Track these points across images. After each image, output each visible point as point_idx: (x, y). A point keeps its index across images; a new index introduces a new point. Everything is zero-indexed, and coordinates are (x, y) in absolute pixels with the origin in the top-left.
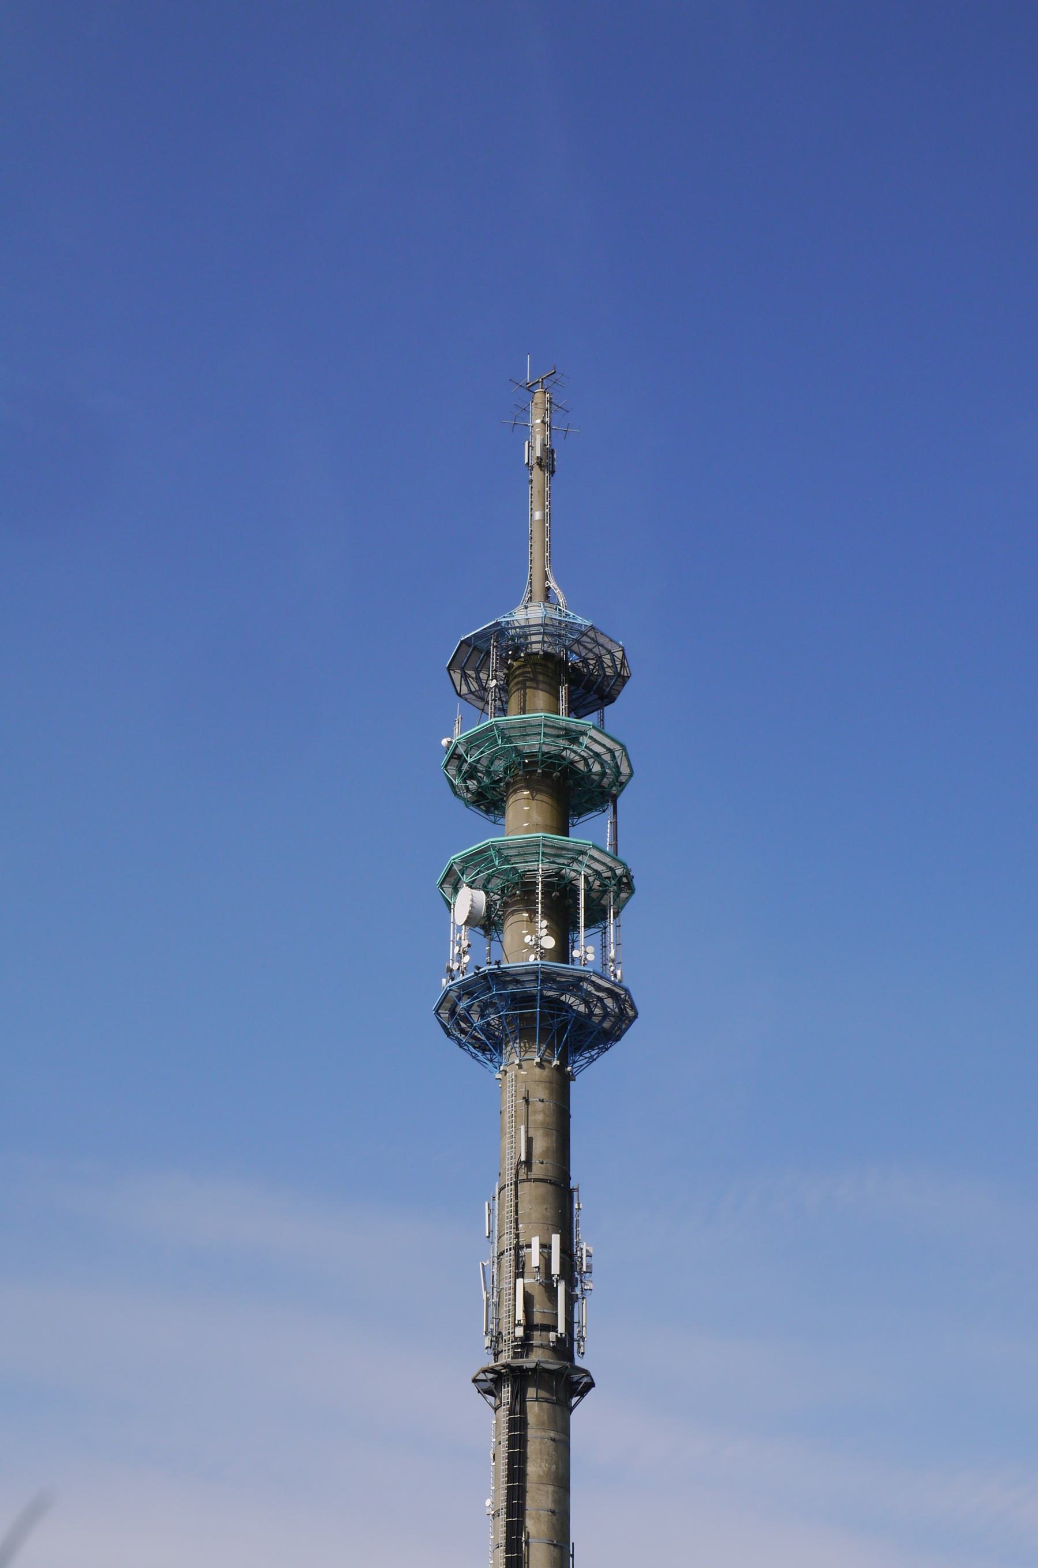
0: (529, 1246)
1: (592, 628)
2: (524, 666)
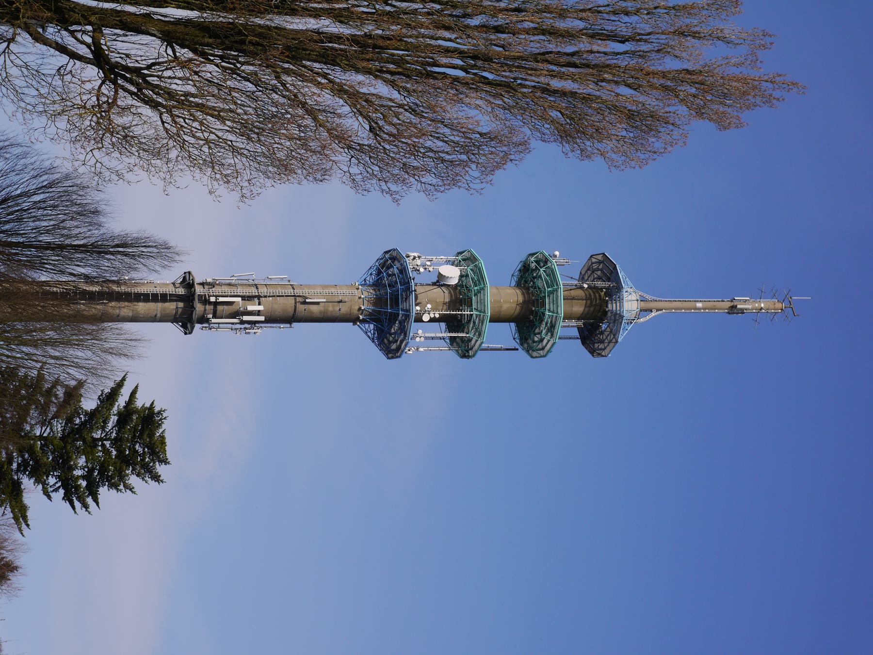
0: (259, 304)
1: (617, 342)
2: (600, 299)
